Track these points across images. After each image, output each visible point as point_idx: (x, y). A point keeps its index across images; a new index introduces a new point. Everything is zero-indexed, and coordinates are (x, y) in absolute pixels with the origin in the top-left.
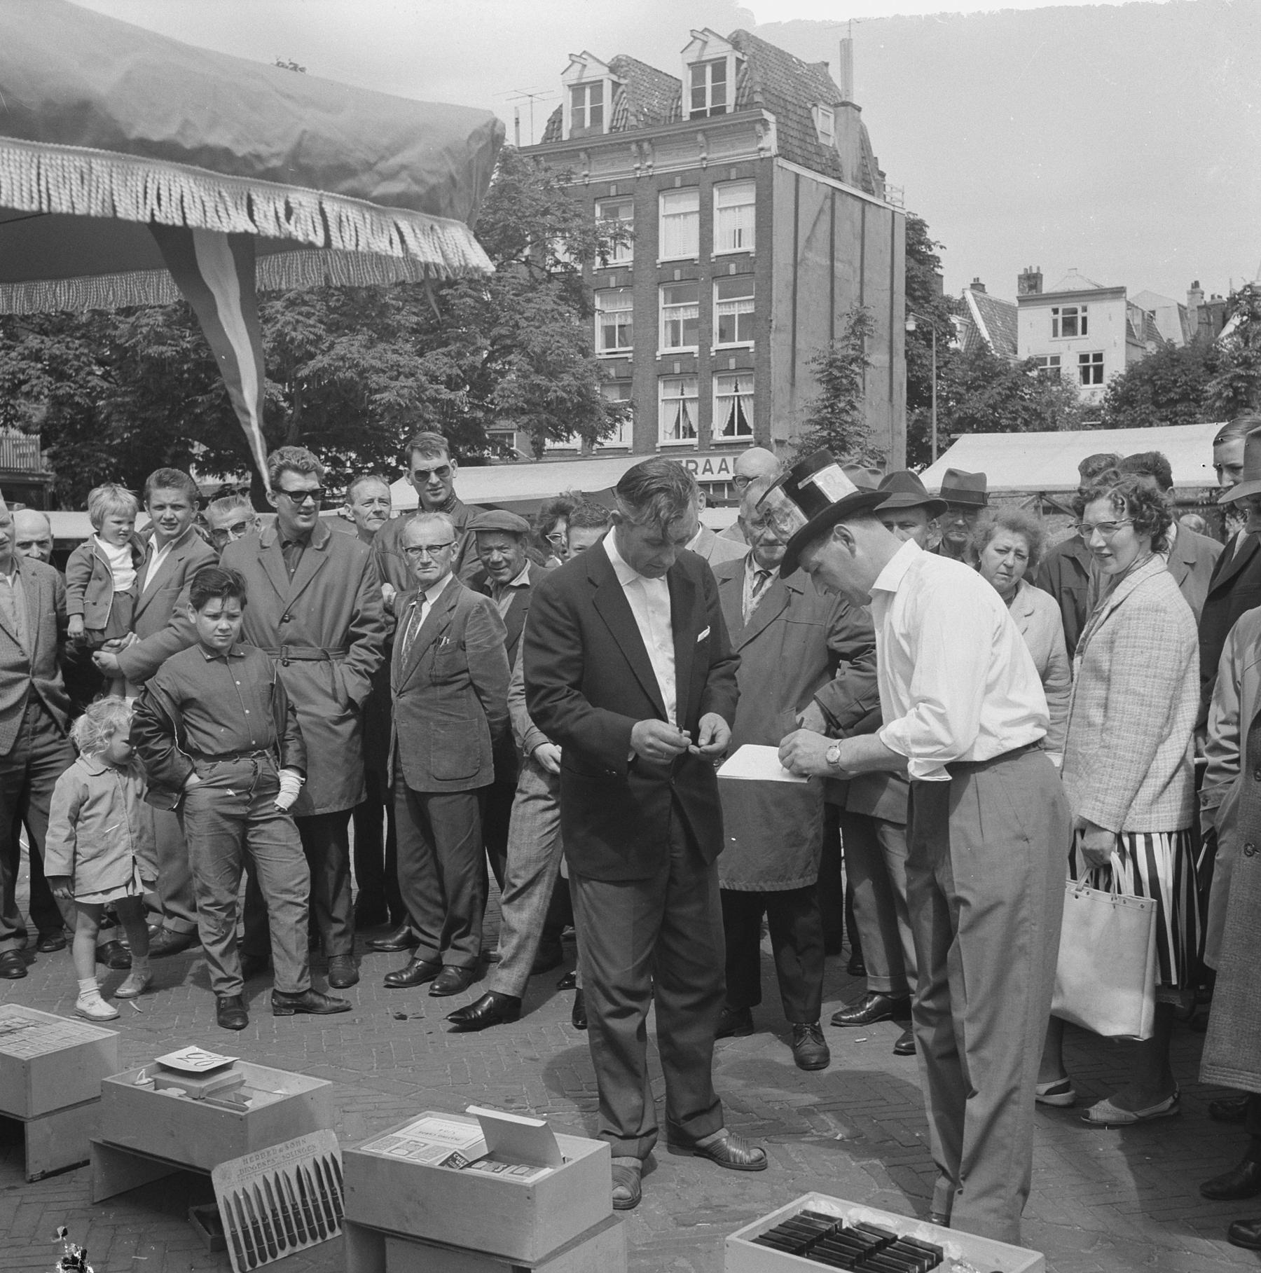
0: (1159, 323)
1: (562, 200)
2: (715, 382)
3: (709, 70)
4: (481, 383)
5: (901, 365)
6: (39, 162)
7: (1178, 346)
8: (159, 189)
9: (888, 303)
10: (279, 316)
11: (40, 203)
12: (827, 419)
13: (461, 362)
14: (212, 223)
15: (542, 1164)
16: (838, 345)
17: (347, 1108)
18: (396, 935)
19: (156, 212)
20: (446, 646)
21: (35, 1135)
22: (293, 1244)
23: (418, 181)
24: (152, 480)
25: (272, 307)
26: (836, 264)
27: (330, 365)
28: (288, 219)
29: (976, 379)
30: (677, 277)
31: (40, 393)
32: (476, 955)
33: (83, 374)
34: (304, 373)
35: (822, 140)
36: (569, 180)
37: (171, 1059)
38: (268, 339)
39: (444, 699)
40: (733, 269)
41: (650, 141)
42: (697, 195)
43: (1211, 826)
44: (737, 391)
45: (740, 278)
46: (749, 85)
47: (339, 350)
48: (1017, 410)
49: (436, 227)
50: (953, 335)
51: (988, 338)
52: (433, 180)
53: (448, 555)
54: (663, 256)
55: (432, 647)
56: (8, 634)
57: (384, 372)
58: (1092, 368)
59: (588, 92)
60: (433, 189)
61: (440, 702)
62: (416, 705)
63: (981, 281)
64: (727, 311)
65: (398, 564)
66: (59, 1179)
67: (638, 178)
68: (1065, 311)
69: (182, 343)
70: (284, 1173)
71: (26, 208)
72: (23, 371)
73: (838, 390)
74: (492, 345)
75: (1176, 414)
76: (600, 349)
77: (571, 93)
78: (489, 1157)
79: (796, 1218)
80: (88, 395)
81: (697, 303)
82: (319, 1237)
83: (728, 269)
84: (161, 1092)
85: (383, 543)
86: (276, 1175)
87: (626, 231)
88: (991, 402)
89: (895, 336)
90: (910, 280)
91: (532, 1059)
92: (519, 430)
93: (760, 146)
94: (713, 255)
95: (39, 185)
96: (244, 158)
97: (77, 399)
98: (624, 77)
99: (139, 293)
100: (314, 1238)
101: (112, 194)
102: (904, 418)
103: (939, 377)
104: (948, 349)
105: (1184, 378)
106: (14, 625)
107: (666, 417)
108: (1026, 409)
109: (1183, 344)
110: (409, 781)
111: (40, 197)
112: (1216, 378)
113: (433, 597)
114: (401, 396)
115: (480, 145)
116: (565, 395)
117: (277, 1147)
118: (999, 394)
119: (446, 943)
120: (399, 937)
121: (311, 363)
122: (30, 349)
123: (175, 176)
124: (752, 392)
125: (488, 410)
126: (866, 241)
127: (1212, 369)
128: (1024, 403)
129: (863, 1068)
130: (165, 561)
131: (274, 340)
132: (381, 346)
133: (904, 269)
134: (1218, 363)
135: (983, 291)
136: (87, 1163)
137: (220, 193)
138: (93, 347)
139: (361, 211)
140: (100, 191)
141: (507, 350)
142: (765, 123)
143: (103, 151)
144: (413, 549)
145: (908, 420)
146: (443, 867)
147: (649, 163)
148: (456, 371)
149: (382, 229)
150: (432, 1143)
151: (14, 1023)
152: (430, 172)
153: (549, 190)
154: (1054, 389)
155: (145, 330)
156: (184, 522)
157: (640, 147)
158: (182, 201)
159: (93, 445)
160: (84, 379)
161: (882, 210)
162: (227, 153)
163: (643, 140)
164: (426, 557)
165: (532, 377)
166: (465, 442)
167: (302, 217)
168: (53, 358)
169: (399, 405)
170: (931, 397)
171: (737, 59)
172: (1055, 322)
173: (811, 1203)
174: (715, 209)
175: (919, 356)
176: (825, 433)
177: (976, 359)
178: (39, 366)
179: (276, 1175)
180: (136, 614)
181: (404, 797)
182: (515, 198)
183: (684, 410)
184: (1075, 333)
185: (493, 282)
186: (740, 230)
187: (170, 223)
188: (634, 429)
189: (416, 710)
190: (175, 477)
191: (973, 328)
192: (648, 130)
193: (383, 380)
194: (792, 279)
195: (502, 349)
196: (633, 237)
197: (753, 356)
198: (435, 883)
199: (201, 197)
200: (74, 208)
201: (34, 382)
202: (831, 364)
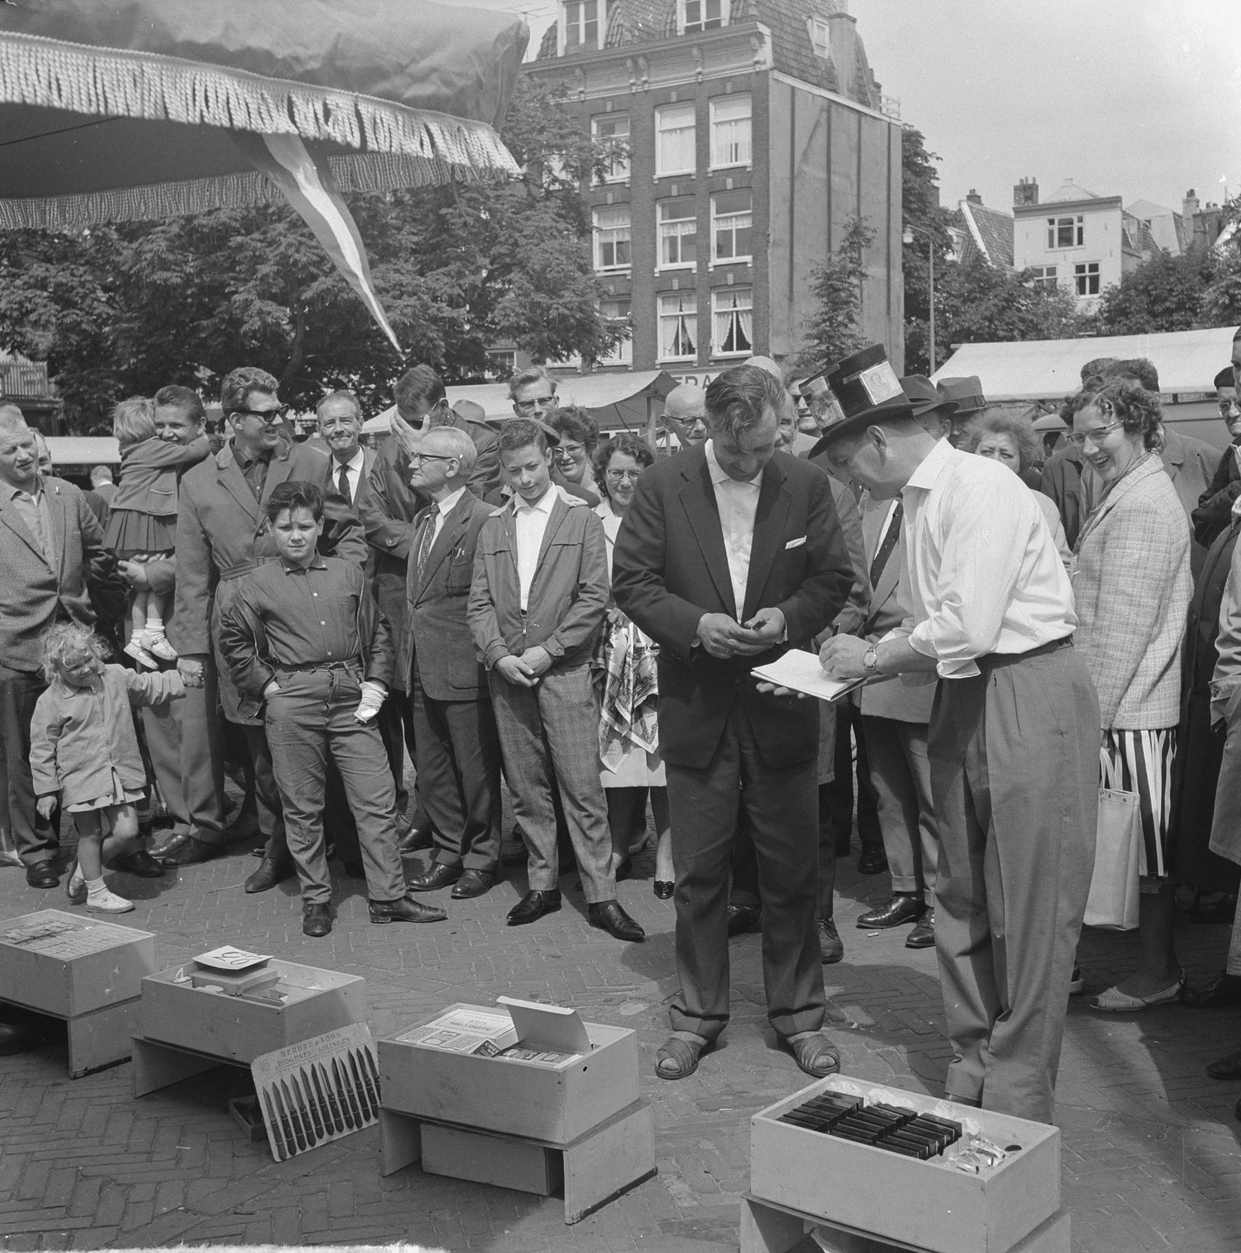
0: (1155, 233)
1: (558, 117)
2: (714, 297)
4: (481, 302)
5: (898, 278)
6: (95, 66)
7: (1173, 255)
8: (206, 91)
9: (885, 215)
10: (282, 238)
11: (98, 105)
12: (825, 332)
13: (462, 282)
15: (568, 1050)
16: (835, 259)
19: (205, 114)
20: (461, 557)
21: (78, 1033)
22: (331, 1133)
23: (447, 83)
25: (274, 230)
26: (832, 177)
27: (334, 286)
28: (326, 121)
30: (674, 193)
31: (48, 322)
32: (496, 858)
33: (88, 301)
34: (307, 295)
35: (817, 52)
37: (208, 958)
40: (730, 183)
41: (645, 56)
42: (693, 110)
43: (1221, 717)
44: (735, 306)
48: (1014, 322)
50: (949, 247)
51: (983, 249)
52: (461, 83)
54: (660, 172)
56: (35, 553)
58: (1088, 278)
60: (462, 91)
62: (433, 616)
63: (978, 193)
64: (724, 227)
66: (101, 1075)
67: (634, 94)
68: (1061, 222)
71: (85, 110)
72: (30, 300)
74: (492, 264)
75: (1172, 324)
76: (598, 265)
77: (565, 10)
78: (519, 1046)
79: (817, 1098)
80: (95, 321)
81: (694, 218)
82: (355, 1126)
83: (724, 184)
84: (199, 989)
86: (313, 1066)
87: (623, 149)
88: (988, 314)
89: (892, 247)
90: (906, 192)
91: (554, 957)
92: (519, 349)
93: (756, 59)
94: (709, 170)
95: (96, 88)
96: (284, 60)
97: (84, 326)
99: (170, 204)
100: (350, 1126)
101: (163, 97)
102: (902, 330)
103: (936, 289)
104: (944, 261)
105: (1179, 287)
106: (41, 545)
107: (665, 334)
108: (1022, 320)
109: (1178, 253)
110: (427, 690)
111: (98, 100)
112: (1211, 286)
114: (405, 315)
115: (506, 48)
116: (567, 312)
118: (995, 305)
119: (466, 847)
121: (315, 285)
122: (36, 278)
123: (220, 79)
124: (751, 308)
125: (489, 330)
127: (1208, 278)
128: (1020, 315)
129: (876, 961)
131: (277, 264)
132: (382, 267)
133: (901, 180)
134: (1214, 271)
135: (979, 202)
136: (128, 1059)
138: (98, 273)
141: (507, 268)
142: (760, 36)
143: (153, 54)
145: (905, 333)
146: (462, 774)
147: (644, 78)
148: (457, 291)
149: (413, 131)
150: (463, 1033)
151: (53, 927)
152: (459, 75)
153: (545, 107)
154: (1051, 299)
155: (149, 256)
157: (635, 63)
158: (228, 103)
159: (100, 372)
160: (90, 307)
161: (878, 122)
162: (268, 55)
166: (465, 362)
168: (59, 285)
169: (404, 323)
170: (928, 310)
172: (1051, 233)
173: (833, 1083)
174: (711, 123)
175: (916, 269)
176: (823, 347)
178: (45, 294)
179: (313, 1066)
182: (513, 116)
183: (683, 326)
185: (492, 200)
186: (736, 145)
187: (218, 124)
188: (634, 348)
189: (433, 621)
192: (643, 45)
194: (789, 193)
195: (501, 269)
196: (630, 156)
197: (751, 272)
198: (455, 790)
199: (245, 99)
200: (129, 110)
202: (828, 277)
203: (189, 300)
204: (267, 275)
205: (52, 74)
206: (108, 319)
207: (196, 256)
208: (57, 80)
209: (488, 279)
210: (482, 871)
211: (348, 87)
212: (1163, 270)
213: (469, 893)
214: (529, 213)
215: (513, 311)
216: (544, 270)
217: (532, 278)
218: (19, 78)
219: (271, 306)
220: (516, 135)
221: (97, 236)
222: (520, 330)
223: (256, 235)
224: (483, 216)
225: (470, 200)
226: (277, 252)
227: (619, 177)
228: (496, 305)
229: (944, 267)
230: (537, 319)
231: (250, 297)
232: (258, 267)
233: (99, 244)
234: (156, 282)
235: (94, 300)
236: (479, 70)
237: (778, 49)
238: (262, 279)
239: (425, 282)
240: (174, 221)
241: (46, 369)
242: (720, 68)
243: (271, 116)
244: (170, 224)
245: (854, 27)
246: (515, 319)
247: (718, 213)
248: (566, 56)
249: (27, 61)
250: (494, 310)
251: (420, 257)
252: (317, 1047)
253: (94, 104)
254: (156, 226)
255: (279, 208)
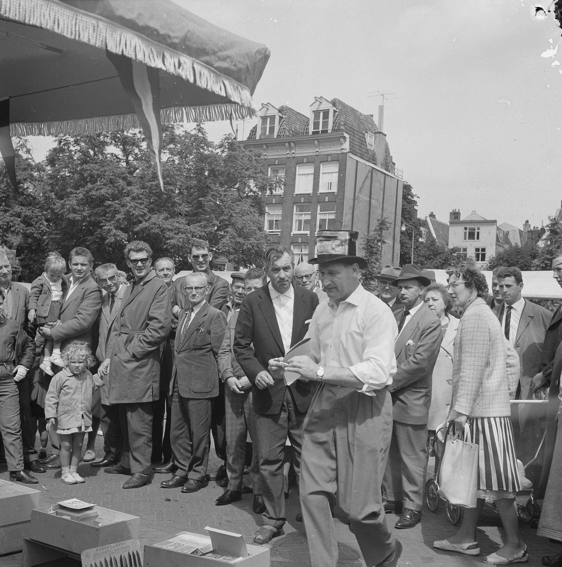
0: (510, 237)
3: (321, 114)
5: (398, 246)
6: (76, 18)
8: (126, 41)
11: (75, 36)
14: (148, 62)
15: (238, 556)
17: (143, 536)
18: (166, 466)
19: (124, 51)
20: (202, 332)
23: (235, 65)
24: (73, 252)
25: (125, 200)
27: (149, 226)
29: (430, 255)
30: (302, 201)
31: (19, 231)
33: (38, 224)
34: (137, 229)
35: (369, 147)
36: (259, 157)
37: (65, 503)
38: (122, 214)
39: (199, 356)
41: (294, 142)
45: (329, 203)
46: (338, 122)
47: (153, 220)
49: (239, 88)
50: (421, 236)
52: (240, 66)
53: (204, 291)
54: (296, 192)
55: (195, 332)
57: (172, 231)
58: (481, 254)
59: (269, 120)
60: (240, 70)
61: (197, 357)
63: (434, 214)
64: (323, 217)
65: (182, 298)
66: (6, 558)
67: (288, 158)
68: (469, 229)
69: (83, 213)
70: (114, 558)
71: (69, 36)
72: (12, 221)
73: (372, 253)
77: (261, 120)
78: (213, 552)
80: (40, 233)
81: (310, 213)
83: (325, 199)
85: (176, 288)
86: (111, 558)
87: (281, 181)
90: (404, 210)
93: (342, 147)
94: (318, 193)
95: (75, 27)
96: (163, 35)
97: (35, 235)
98: (285, 115)
101: (106, 39)
111: (76, 33)
113: (196, 310)
114: (179, 242)
117: (112, 545)
118: (440, 262)
119: (190, 468)
120: (168, 467)
121: (140, 225)
126: (386, 191)
127: (534, 257)
130: (76, 289)
131: (125, 214)
135: (435, 218)
136: (21, 551)
137: (151, 49)
139: (209, 72)
140: (101, 36)
141: (227, 226)
142: (345, 138)
144: (189, 288)
147: (293, 152)
148: (203, 234)
150: (186, 545)
152: (240, 62)
155: (68, 207)
156: (86, 272)
157: (290, 145)
158: (135, 48)
161: (393, 179)
163: (291, 142)
164: (194, 292)
165: (237, 238)
167: (185, 68)
169: (178, 245)
171: (334, 110)
172: (465, 233)
175: (406, 244)
177: (430, 246)
178: (19, 219)
179: (111, 558)
180: (61, 311)
181: (177, 400)
182: (235, 162)
183: (302, 258)
184: (474, 239)
186: (331, 183)
189: (186, 360)
190: (84, 251)
191: (429, 233)
192: (294, 138)
193: (171, 234)
195: (223, 226)
196: (285, 185)
200: (89, 41)
201: (17, 226)
203: (84, 228)
204: (119, 219)
205: (56, 17)
206: (46, 233)
207: (89, 208)
208: (58, 20)
209: (217, 230)
210: (196, 480)
211: (190, 55)
212: (515, 252)
213: (189, 490)
214: (238, 203)
215: (228, 244)
216: (243, 228)
217: (237, 231)
218: (41, 15)
219: (120, 233)
220: (236, 170)
221: (46, 196)
222: (229, 253)
223: (117, 202)
224: (218, 202)
225: (213, 195)
226: (125, 209)
227: (280, 192)
228: (220, 241)
229: (418, 244)
230: (238, 249)
231: (111, 228)
232: (116, 215)
233: (46, 200)
234: (69, 218)
235: (41, 224)
236: (249, 63)
237: (352, 144)
238: (117, 221)
239: (189, 228)
240: (81, 192)
241: (15, 253)
242: (328, 150)
243: (154, 60)
244: (79, 193)
245: (385, 139)
246: (228, 248)
247: (321, 211)
248: (260, 139)
249: (46, 8)
250: (219, 244)
251: (189, 218)
252: (114, 548)
253: (73, 35)
254: (72, 194)
255: (128, 191)
